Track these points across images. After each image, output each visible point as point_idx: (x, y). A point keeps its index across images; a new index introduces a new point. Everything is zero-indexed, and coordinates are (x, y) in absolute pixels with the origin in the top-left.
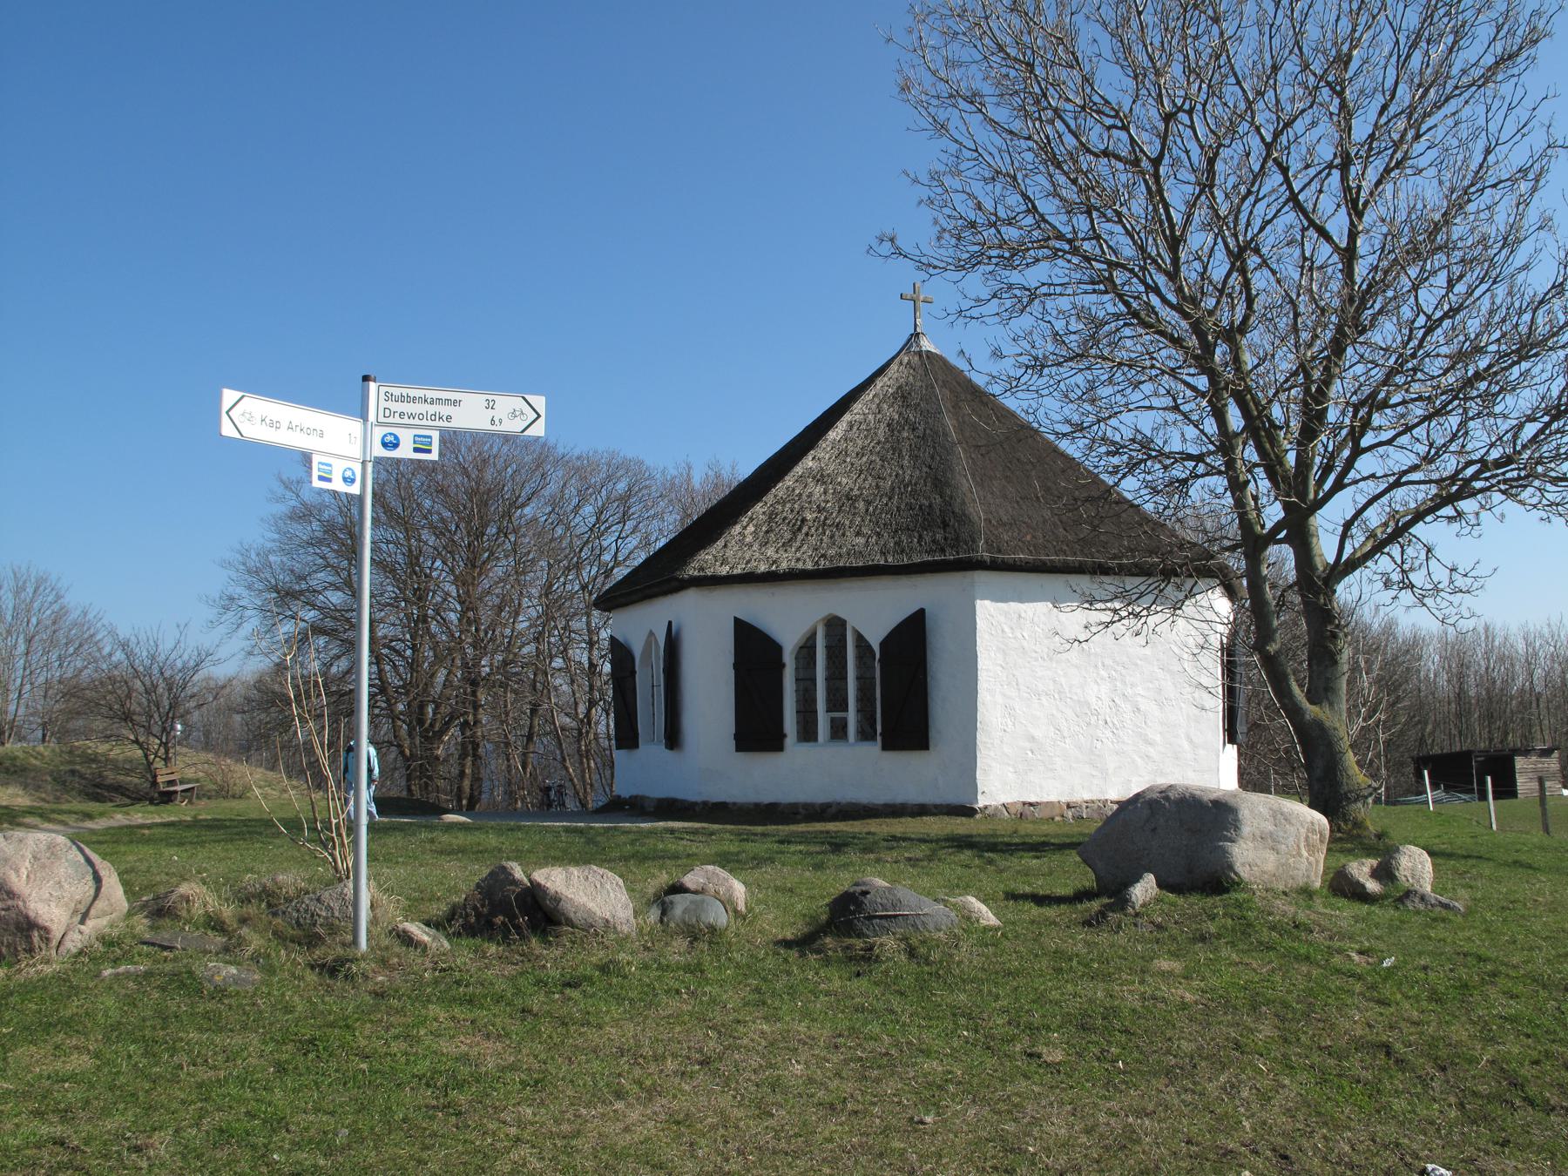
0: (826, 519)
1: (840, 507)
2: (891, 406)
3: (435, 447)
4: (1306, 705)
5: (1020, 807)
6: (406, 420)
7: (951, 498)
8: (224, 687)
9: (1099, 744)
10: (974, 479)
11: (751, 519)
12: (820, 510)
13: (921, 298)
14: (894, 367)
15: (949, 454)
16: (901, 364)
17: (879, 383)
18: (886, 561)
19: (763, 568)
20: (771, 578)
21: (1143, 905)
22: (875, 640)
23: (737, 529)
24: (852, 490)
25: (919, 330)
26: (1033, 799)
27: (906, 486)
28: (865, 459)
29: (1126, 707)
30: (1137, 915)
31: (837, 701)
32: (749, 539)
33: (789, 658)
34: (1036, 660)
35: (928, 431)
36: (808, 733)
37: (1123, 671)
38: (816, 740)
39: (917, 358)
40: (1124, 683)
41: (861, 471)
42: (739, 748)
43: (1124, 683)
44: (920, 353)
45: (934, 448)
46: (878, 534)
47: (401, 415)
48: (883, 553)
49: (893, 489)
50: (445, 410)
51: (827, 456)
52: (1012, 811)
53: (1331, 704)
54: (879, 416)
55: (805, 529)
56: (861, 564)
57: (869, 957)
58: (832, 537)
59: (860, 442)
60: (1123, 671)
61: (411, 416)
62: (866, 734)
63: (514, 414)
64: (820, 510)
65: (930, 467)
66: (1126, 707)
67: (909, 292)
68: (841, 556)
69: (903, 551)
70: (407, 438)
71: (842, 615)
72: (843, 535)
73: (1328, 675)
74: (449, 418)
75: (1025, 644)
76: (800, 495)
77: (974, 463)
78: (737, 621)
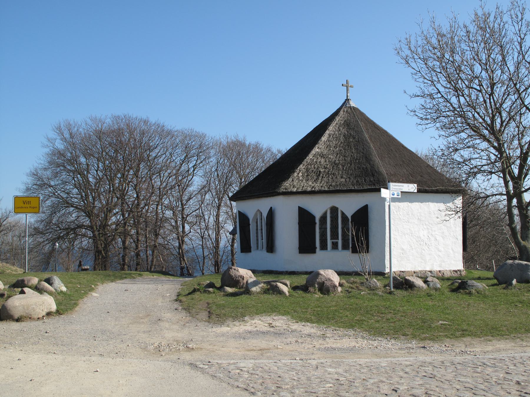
0: (328, 172)
1: (333, 167)
2: (343, 128)
3: (400, 195)
4: (521, 241)
5: (399, 273)
6: (396, 190)
7: (373, 165)
8: (14, 226)
9: (424, 251)
10: (379, 158)
11: (300, 171)
12: (325, 168)
13: (349, 86)
14: (341, 112)
15: (369, 148)
16: (344, 111)
17: (338, 118)
18: (355, 188)
19: (309, 189)
20: (313, 193)
21: (515, 285)
22: (349, 215)
23: (296, 174)
24: (335, 161)
25: (348, 98)
26: (403, 270)
27: (356, 160)
28: (338, 149)
29: (432, 239)
30: (514, 287)
31: (334, 235)
32: (301, 178)
33: (317, 221)
34: (404, 222)
35: (360, 139)
36: (324, 247)
37: (432, 226)
38: (326, 249)
39: (350, 109)
40: (432, 230)
41: (337, 154)
42: (250, 251)
43: (432, 230)
44: (350, 107)
45: (363, 146)
46: (349, 178)
47: (395, 189)
48: (353, 185)
49: (351, 161)
50: (401, 187)
51: (323, 147)
52: (397, 274)
53: (528, 241)
54: (340, 132)
55: (321, 175)
56: (345, 189)
57: (470, 294)
58: (332, 178)
59: (334, 142)
60: (432, 226)
61: (396, 189)
62: (345, 247)
63: (412, 188)
64: (325, 168)
65: (363, 153)
66: (432, 239)
67: (345, 83)
68: (337, 185)
69: (360, 184)
70: (396, 193)
71: (337, 206)
72: (336, 178)
73: (527, 233)
74: (402, 189)
75: (400, 217)
76: (316, 162)
77: (378, 152)
78: (299, 207)
